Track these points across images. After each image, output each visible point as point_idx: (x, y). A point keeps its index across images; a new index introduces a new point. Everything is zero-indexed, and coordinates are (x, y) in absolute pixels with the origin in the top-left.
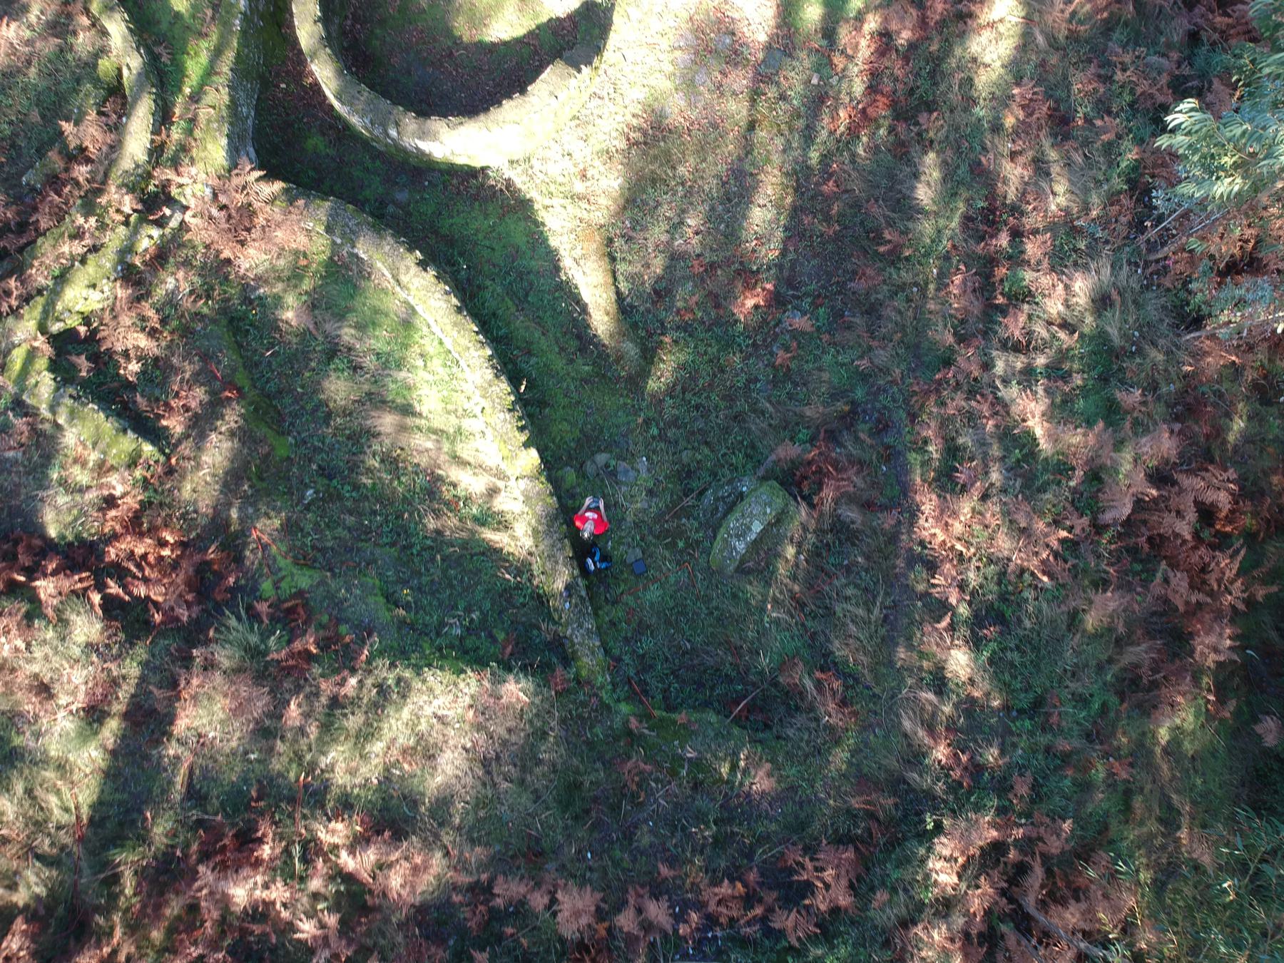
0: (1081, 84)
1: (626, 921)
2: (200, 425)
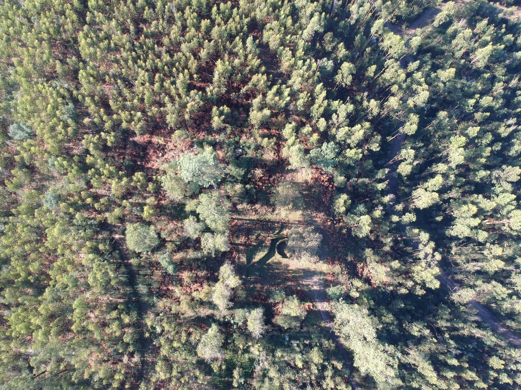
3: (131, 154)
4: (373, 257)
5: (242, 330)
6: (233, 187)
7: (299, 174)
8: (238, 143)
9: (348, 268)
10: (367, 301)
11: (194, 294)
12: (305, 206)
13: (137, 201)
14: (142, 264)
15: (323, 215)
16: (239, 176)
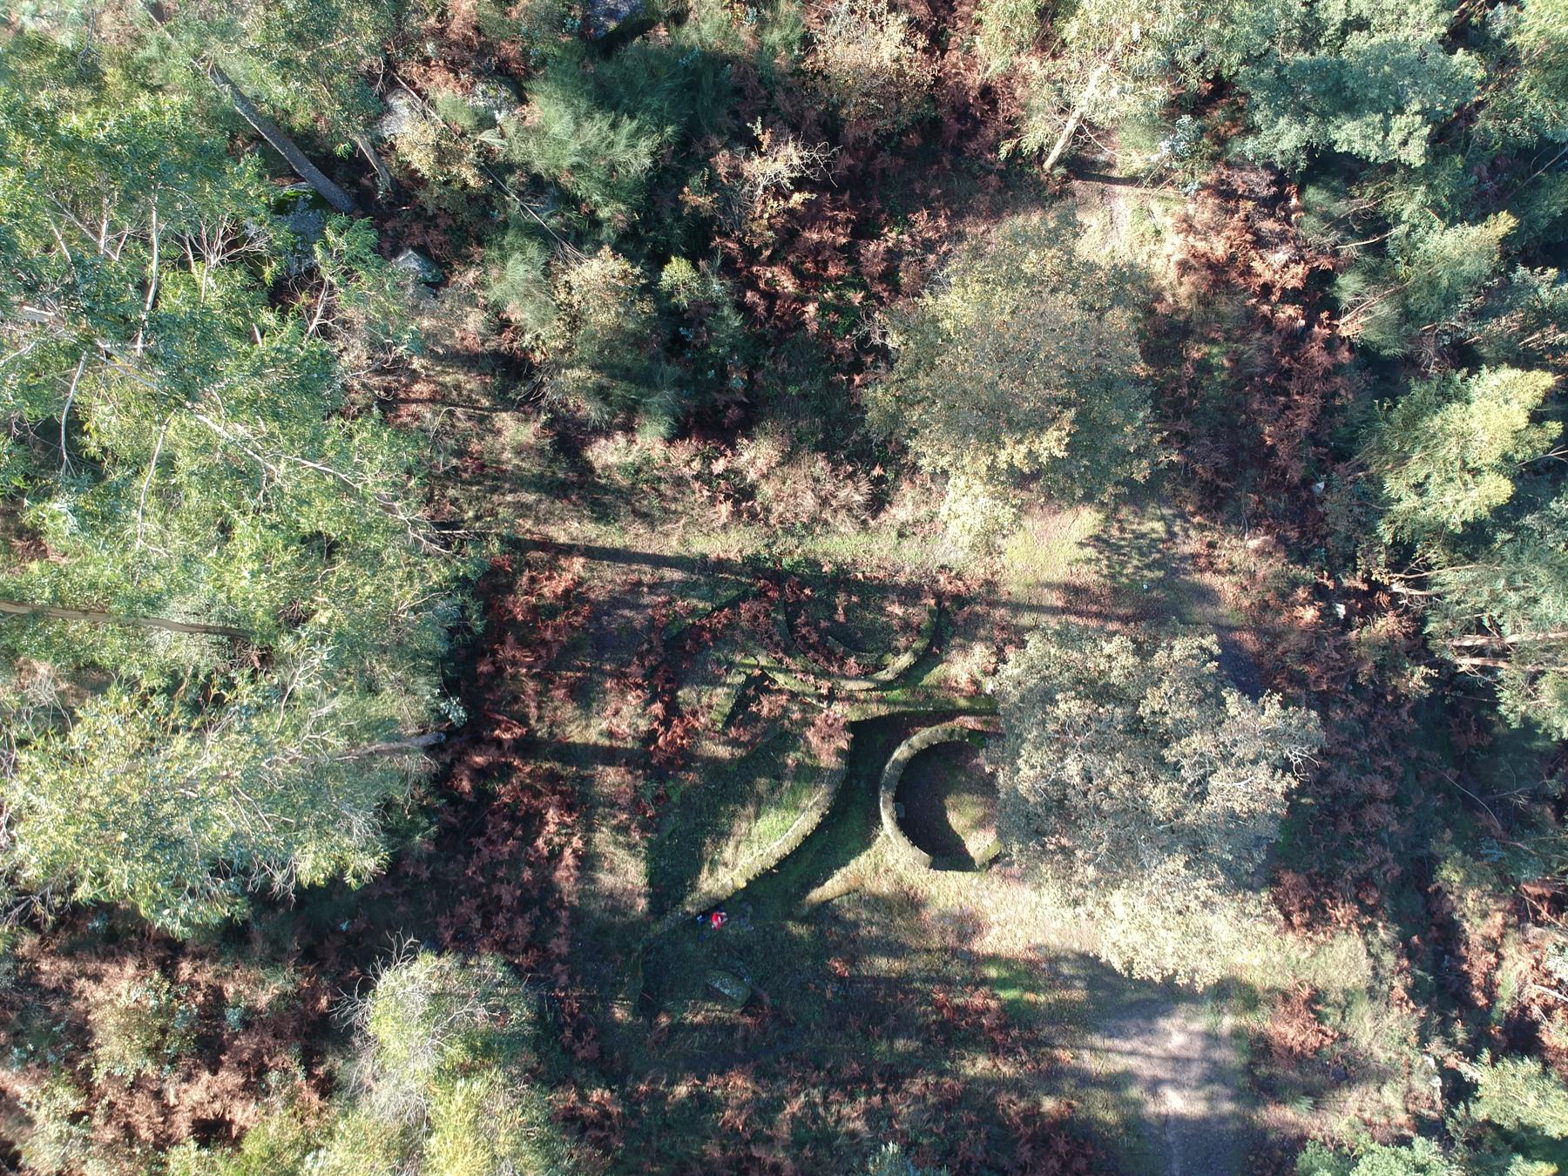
0: (966, 1115)
1: (558, 967)
2: (734, 743)
15: (1261, 553)
16: (612, 189)
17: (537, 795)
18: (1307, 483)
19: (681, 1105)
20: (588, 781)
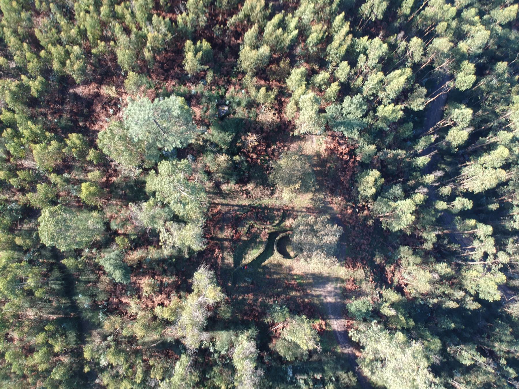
2: (248, 237)
3: (71, 111)
4: (411, 259)
5: (226, 360)
6: (214, 159)
7: (309, 143)
8: (222, 97)
9: (374, 273)
10: (404, 321)
11: (158, 310)
12: (318, 187)
13: (77, 177)
14: (80, 266)
15: (341, 200)
16: (224, 143)
17: (214, 247)
18: (349, 187)
19: (241, 300)
20: (223, 244)
